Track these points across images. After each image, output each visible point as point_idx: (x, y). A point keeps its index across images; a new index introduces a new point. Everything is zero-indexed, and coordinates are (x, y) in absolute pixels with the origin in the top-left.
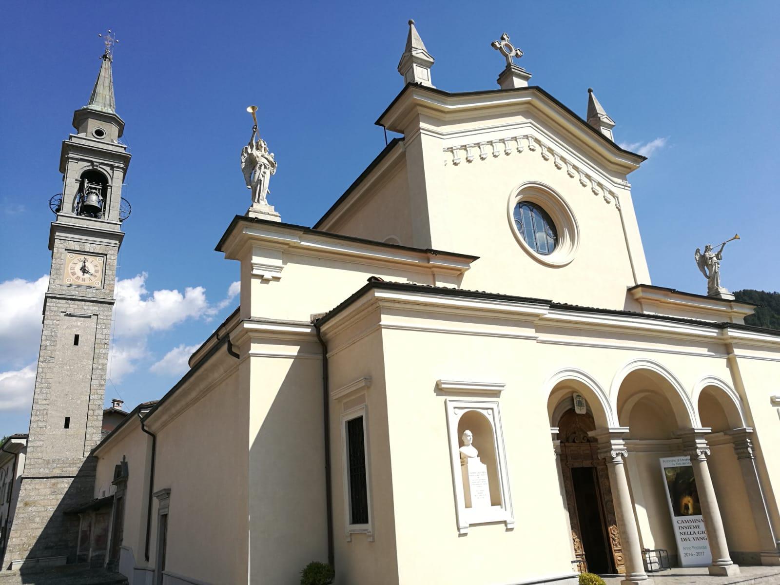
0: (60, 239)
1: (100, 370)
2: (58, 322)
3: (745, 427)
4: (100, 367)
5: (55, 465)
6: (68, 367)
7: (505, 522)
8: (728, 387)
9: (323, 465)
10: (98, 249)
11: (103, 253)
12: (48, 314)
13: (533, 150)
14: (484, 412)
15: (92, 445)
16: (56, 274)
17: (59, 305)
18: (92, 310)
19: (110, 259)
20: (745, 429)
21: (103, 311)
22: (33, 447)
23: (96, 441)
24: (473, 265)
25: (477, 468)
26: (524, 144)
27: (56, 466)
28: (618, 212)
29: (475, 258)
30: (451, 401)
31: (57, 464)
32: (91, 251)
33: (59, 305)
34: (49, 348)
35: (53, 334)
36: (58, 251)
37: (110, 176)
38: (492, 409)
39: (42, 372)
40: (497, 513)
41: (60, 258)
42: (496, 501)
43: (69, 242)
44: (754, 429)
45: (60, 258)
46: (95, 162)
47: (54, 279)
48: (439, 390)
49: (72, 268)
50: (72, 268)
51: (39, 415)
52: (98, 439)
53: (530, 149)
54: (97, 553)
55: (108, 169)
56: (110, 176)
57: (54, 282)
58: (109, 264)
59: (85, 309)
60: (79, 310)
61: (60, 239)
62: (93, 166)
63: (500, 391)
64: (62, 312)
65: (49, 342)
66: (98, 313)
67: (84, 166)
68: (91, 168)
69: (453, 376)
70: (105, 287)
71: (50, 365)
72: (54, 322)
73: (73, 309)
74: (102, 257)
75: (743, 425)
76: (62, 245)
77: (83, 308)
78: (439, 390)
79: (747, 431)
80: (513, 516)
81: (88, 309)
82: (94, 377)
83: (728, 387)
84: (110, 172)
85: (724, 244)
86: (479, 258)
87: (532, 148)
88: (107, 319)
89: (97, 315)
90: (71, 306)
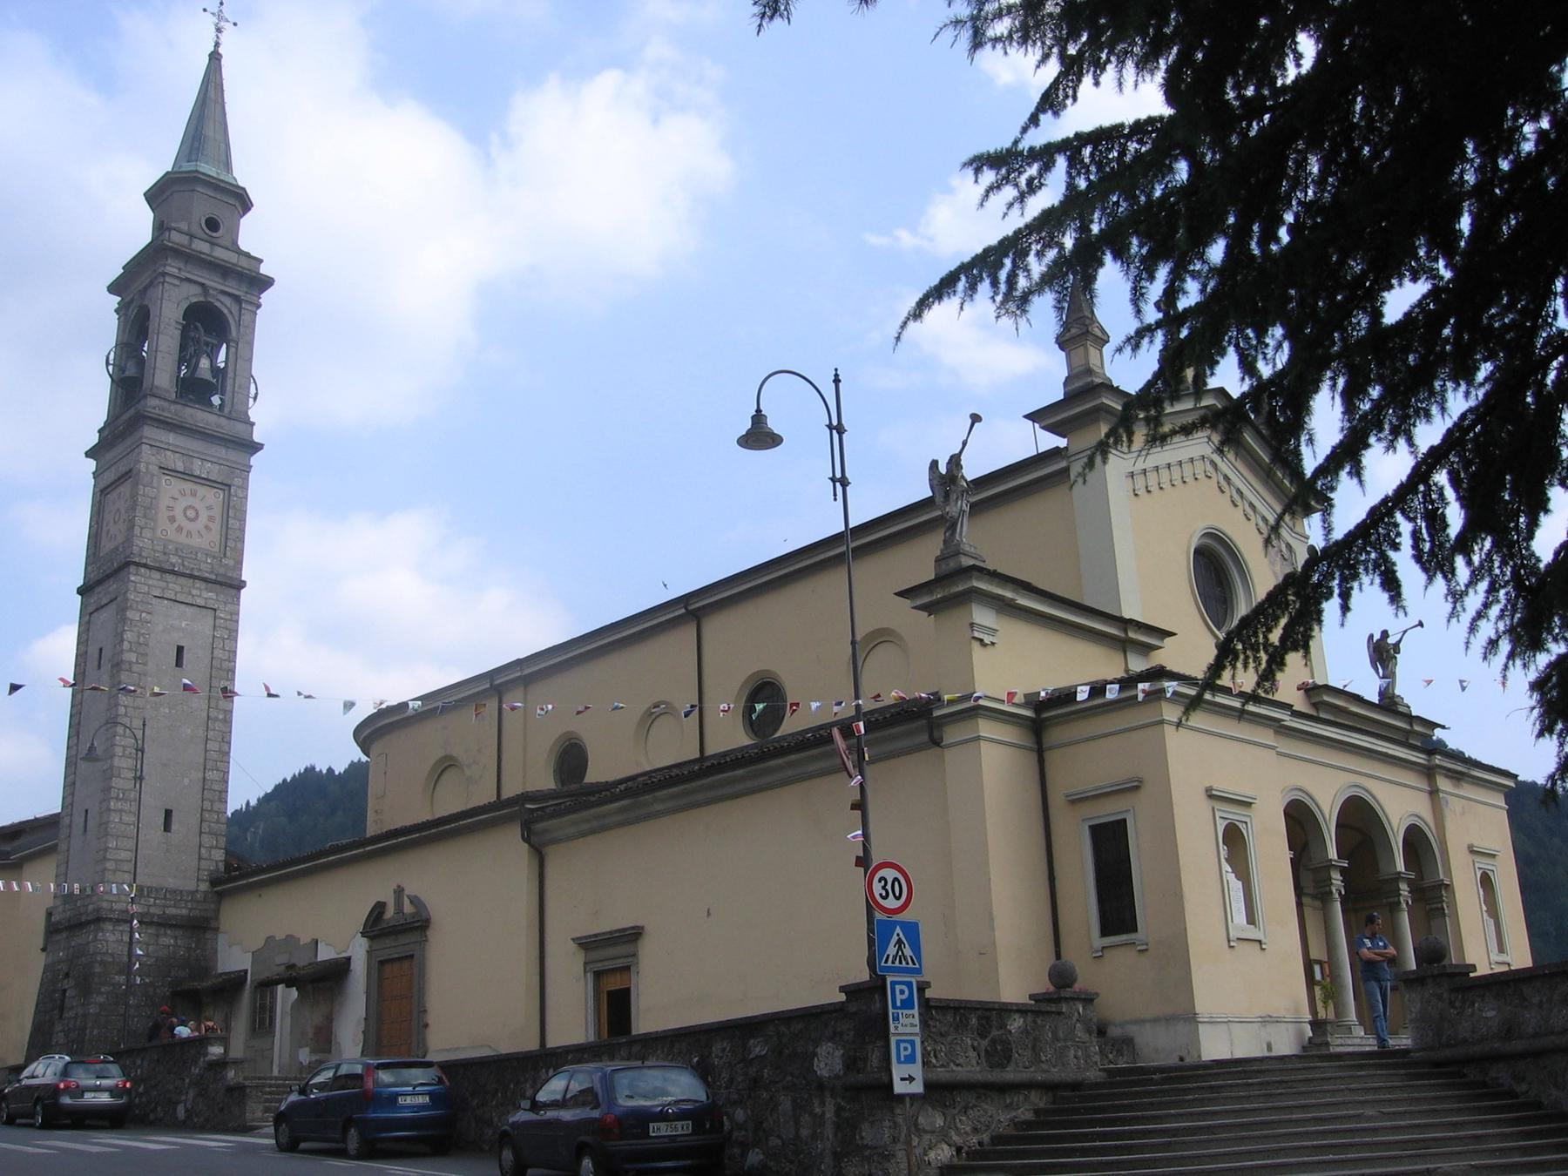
0: (151, 445)
1: (220, 721)
2: (148, 617)
3: (1441, 877)
4: (221, 717)
5: (152, 900)
6: (167, 711)
7: (1260, 942)
8: (1428, 826)
9: (537, 952)
10: (214, 472)
11: (224, 482)
12: (132, 597)
13: (1210, 477)
14: (1240, 825)
15: (212, 868)
16: (145, 517)
17: (150, 582)
18: (206, 599)
19: (236, 496)
20: (1442, 880)
21: (225, 603)
22: (116, 860)
23: (217, 861)
24: (1168, 640)
25: (1236, 886)
26: (1199, 466)
27: (155, 903)
28: (961, 446)
29: (1172, 634)
30: (1219, 810)
31: (155, 899)
32: (203, 476)
33: (150, 582)
34: (135, 668)
35: (142, 640)
36: (147, 468)
37: (234, 317)
38: (1246, 823)
39: (126, 715)
40: (1252, 933)
41: (150, 485)
42: (1251, 919)
43: (167, 452)
44: (1451, 880)
45: (150, 485)
46: (211, 288)
47: (142, 528)
48: (1211, 795)
49: (170, 508)
50: (170, 508)
51: (122, 799)
52: (220, 859)
53: (1207, 476)
54: (318, 1058)
55: (227, 301)
56: (234, 317)
57: (141, 533)
58: (234, 506)
59: (193, 596)
60: (184, 595)
61: (151, 445)
62: (205, 296)
63: (1251, 803)
64: (155, 596)
65: (135, 655)
66: (216, 606)
67: (192, 294)
68: (202, 299)
69: (1224, 786)
70: (228, 554)
71: (139, 702)
72: (144, 615)
73: (173, 593)
74: (221, 489)
75: (1438, 874)
76: (153, 458)
77: (190, 593)
78: (1211, 797)
79: (1445, 882)
80: (1265, 937)
81: (200, 596)
82: (211, 734)
83: (1428, 826)
84: (235, 308)
85: (1405, 632)
86: (1175, 634)
87: (1209, 475)
88: (230, 620)
89: (215, 610)
90: (171, 585)
